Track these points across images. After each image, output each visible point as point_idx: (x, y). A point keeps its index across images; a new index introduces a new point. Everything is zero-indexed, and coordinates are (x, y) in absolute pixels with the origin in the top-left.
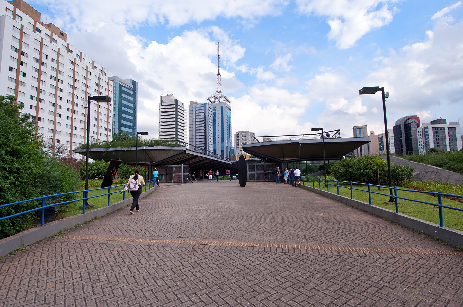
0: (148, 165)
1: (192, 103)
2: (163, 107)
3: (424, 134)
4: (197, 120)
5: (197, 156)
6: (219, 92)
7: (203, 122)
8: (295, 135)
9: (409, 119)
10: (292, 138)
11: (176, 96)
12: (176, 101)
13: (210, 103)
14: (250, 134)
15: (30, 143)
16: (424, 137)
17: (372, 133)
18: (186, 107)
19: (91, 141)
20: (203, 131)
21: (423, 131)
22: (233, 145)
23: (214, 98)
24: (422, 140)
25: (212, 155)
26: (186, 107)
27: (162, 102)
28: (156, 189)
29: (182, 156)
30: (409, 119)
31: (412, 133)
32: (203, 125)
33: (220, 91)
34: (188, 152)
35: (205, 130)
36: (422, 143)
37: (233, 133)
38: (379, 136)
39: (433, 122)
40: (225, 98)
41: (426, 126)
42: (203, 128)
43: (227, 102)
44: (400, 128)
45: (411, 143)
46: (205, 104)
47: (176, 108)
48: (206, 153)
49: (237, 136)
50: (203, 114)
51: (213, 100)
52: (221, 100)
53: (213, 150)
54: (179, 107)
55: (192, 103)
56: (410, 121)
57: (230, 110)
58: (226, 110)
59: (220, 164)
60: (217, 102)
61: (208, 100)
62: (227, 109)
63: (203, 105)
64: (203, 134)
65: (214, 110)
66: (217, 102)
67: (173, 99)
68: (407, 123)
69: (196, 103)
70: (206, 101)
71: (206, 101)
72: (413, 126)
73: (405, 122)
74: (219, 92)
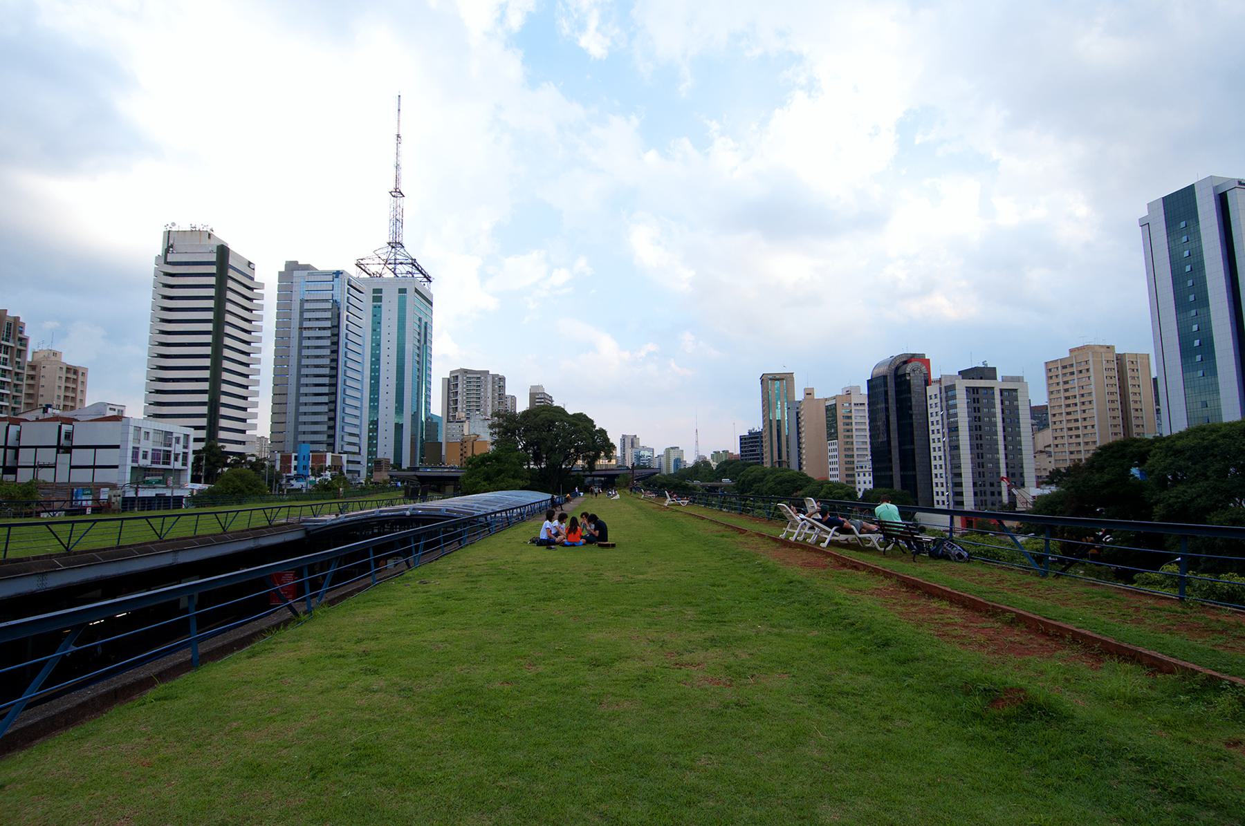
3: (944, 404)
4: (306, 324)
6: (395, 245)
9: (905, 362)
11: (224, 235)
12: (223, 251)
14: (490, 379)
16: (945, 411)
17: (809, 393)
18: (267, 276)
21: (944, 395)
22: (437, 407)
23: (377, 261)
24: (939, 418)
26: (267, 276)
27: (167, 251)
28: (487, 471)
30: (905, 362)
31: (913, 400)
36: (939, 427)
37: (439, 373)
38: (828, 403)
39: (965, 374)
40: (414, 263)
41: (949, 384)
44: (886, 384)
45: (911, 425)
49: (451, 384)
52: (401, 269)
54: (231, 273)
55: (292, 267)
56: (909, 368)
67: (213, 246)
68: (900, 372)
69: (307, 267)
72: (916, 382)
73: (897, 368)
74: (395, 245)
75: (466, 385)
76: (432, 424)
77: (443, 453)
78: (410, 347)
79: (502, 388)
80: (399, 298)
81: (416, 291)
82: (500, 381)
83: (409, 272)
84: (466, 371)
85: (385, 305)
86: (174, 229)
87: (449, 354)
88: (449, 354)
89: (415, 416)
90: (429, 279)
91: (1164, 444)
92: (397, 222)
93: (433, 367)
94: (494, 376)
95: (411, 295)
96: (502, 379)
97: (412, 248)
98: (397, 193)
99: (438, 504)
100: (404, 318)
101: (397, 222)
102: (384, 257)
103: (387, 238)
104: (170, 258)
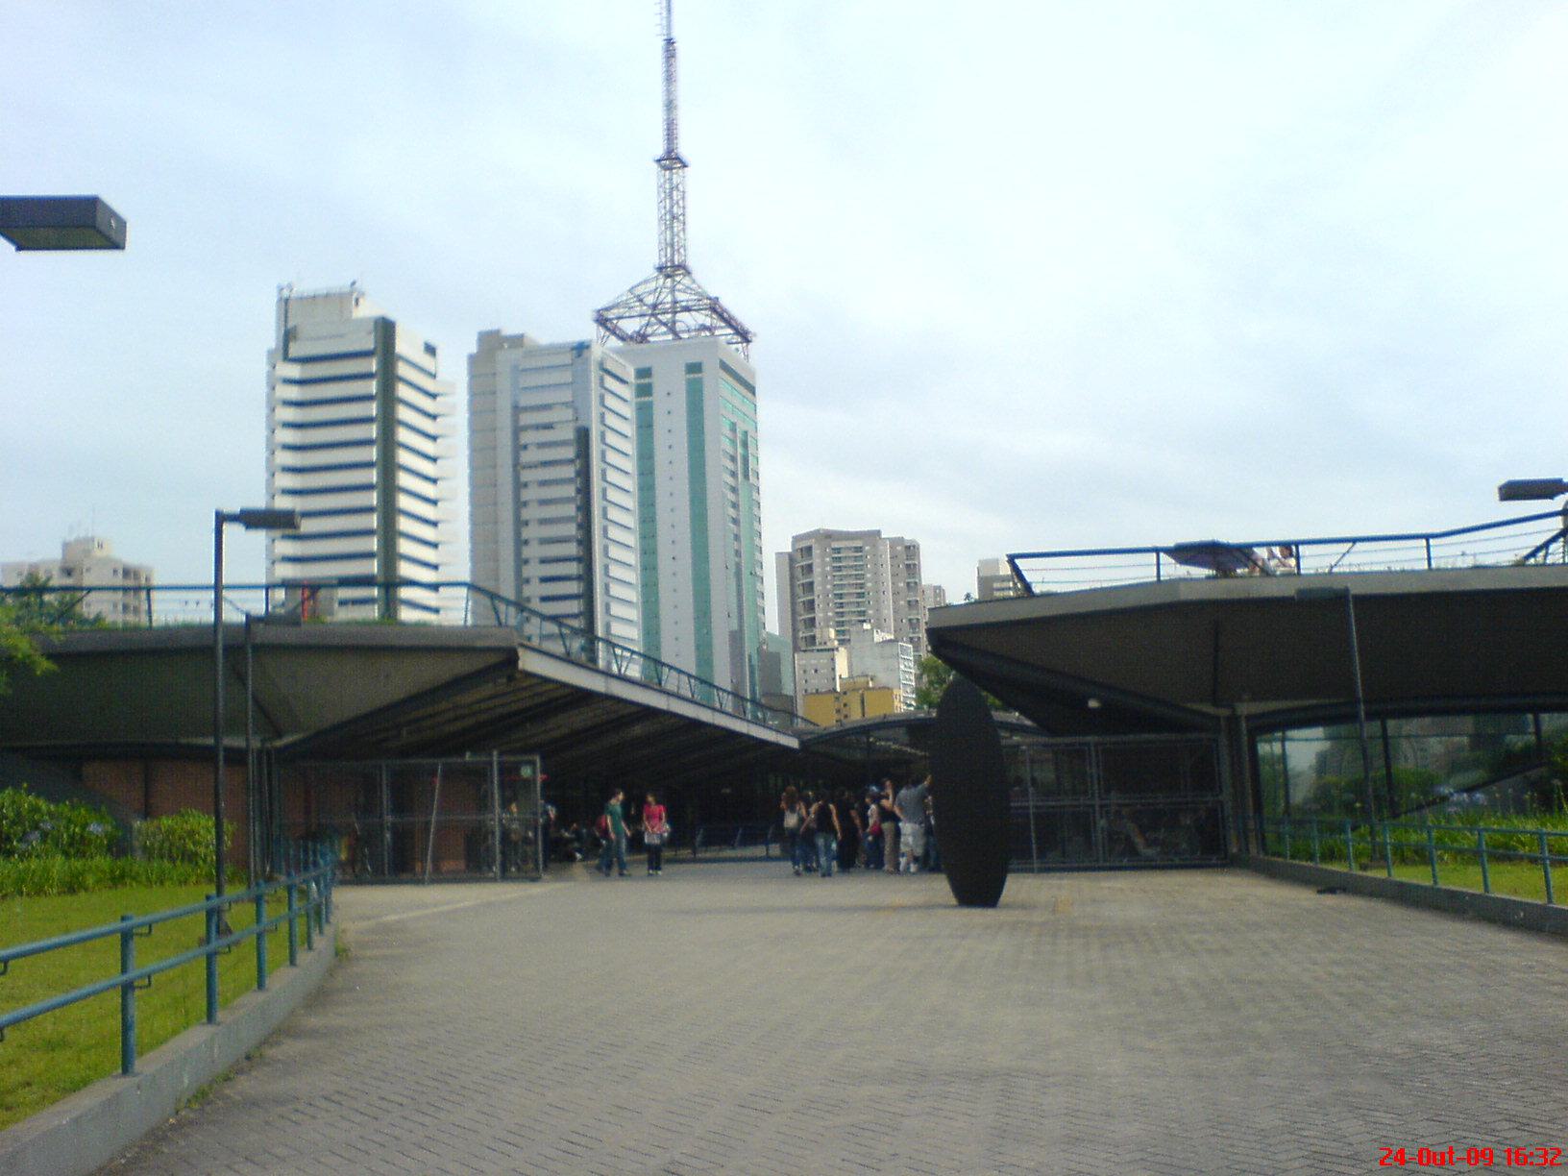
0: (236, 757)
1: (492, 344)
2: (294, 371)
5: (583, 696)
6: (672, 269)
7: (569, 472)
8: (1427, 537)
10: (1409, 558)
13: (614, 342)
15: (305, 894)
19: (1434, 565)
20: (571, 530)
25: (634, 671)
26: (453, 372)
27: (288, 336)
29: (488, 689)
32: (570, 491)
33: (682, 268)
34: (529, 662)
35: (586, 526)
37: (776, 539)
40: (715, 308)
42: (570, 510)
43: (725, 332)
46: (581, 348)
47: (388, 378)
48: (594, 660)
50: (569, 414)
51: (630, 326)
52: (686, 320)
53: (638, 639)
55: (492, 344)
57: (752, 390)
58: (720, 391)
59: (580, 718)
60: (660, 336)
61: (602, 321)
62: (726, 386)
63: (567, 359)
64: (572, 549)
65: (644, 390)
66: (660, 336)
69: (517, 341)
70: (590, 332)
71: (590, 332)
74: (672, 269)
75: (837, 570)
76: (770, 663)
77: (793, 743)
78: (718, 476)
79: (913, 569)
80: (689, 382)
81: (725, 367)
82: (908, 555)
83: (704, 328)
84: (829, 536)
85: (658, 398)
86: (294, 295)
87: (799, 494)
88: (799, 494)
89: (736, 638)
90: (744, 336)
91: (933, 854)
92: (673, 218)
93: (765, 513)
94: (895, 542)
95: (711, 376)
96: (911, 550)
97: (711, 276)
98: (671, 160)
99: (1314, 702)
100: (705, 546)
101: (673, 218)
102: (650, 300)
103: (651, 257)
104: (295, 350)
